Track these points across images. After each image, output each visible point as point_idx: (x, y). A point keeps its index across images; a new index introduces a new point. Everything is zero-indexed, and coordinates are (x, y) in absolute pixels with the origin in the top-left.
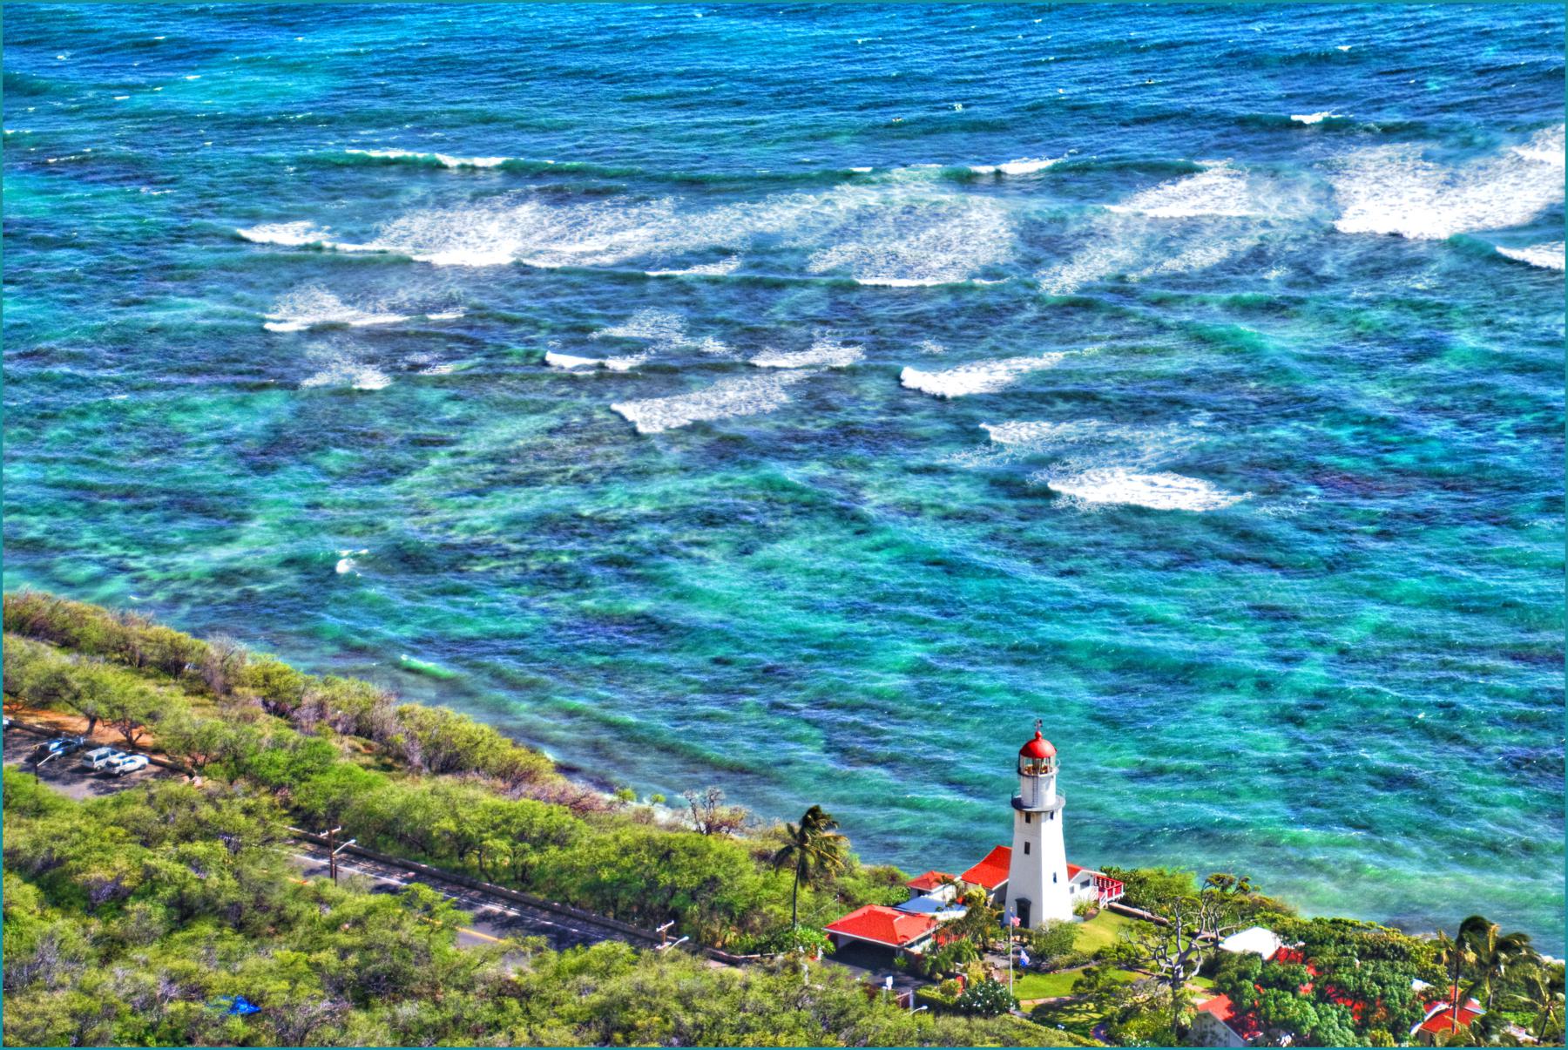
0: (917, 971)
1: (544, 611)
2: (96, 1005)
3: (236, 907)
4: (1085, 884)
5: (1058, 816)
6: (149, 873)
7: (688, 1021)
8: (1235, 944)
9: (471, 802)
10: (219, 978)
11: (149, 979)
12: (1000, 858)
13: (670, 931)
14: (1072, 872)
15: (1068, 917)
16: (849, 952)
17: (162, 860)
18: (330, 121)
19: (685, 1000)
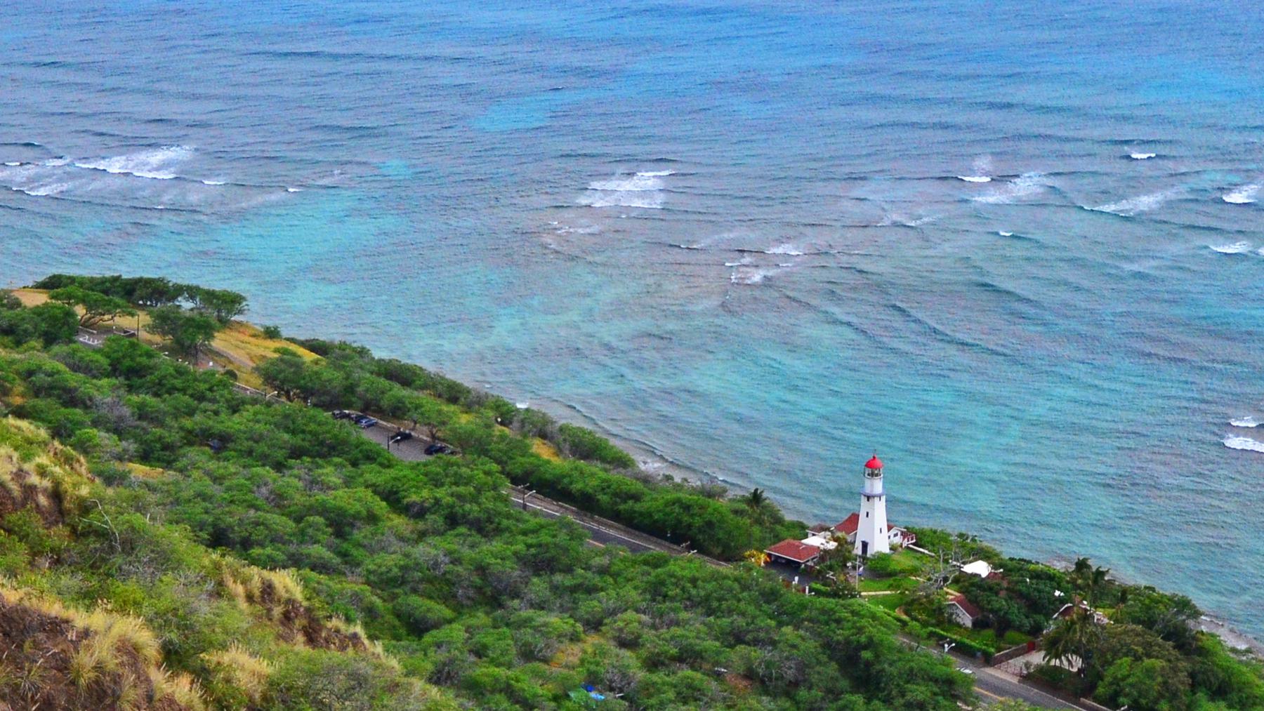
2: (411, 563)
3: (478, 520)
4: (896, 535)
5: (883, 499)
6: (437, 501)
7: (694, 592)
8: (969, 568)
9: (593, 475)
10: (466, 552)
15: (886, 550)
17: (440, 493)
18: (968, 128)
19: (694, 581)
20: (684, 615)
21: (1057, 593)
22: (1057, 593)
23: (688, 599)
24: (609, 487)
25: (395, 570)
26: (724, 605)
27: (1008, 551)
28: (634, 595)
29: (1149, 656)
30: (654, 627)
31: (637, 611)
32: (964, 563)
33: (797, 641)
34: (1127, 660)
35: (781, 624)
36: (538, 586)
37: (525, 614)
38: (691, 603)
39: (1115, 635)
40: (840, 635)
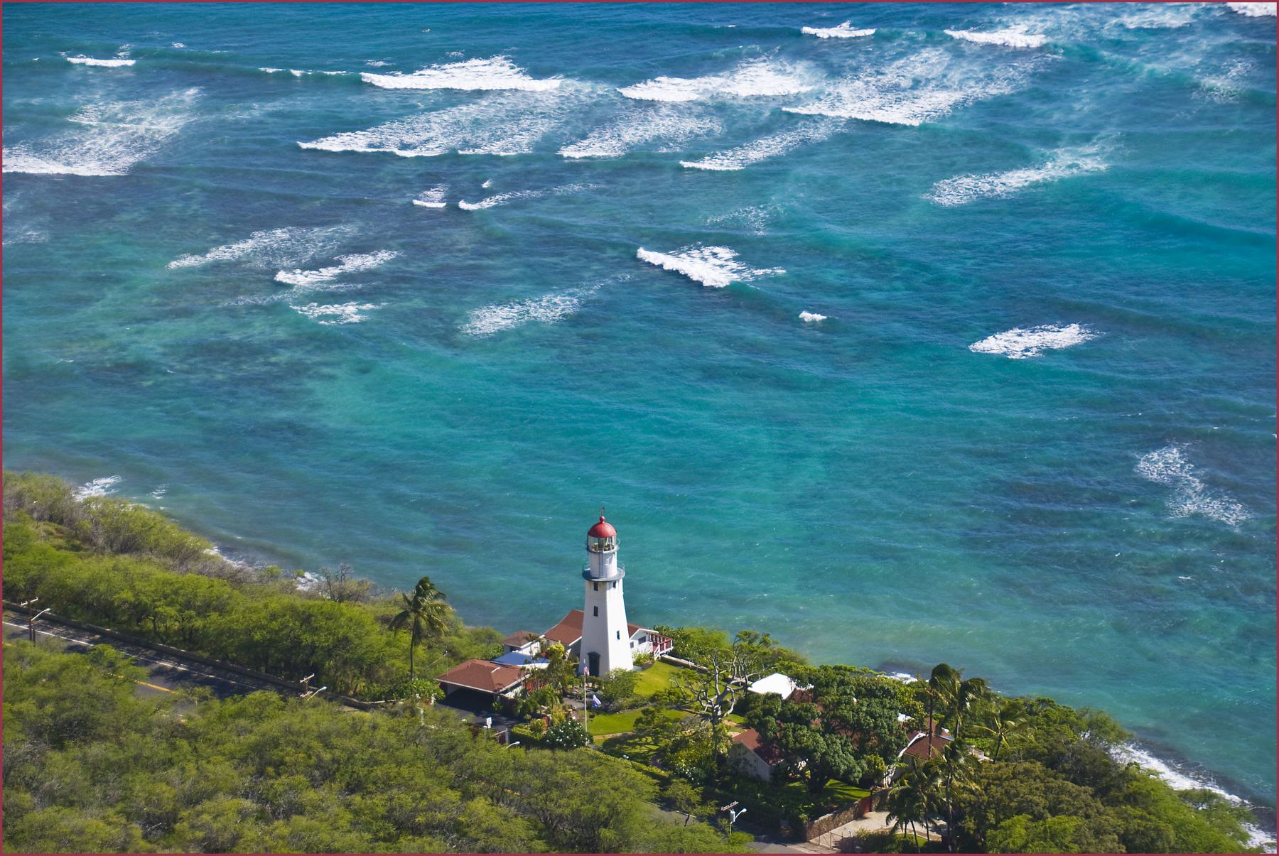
0: (509, 712)
5: (620, 585)
7: (327, 756)
12: (575, 620)
13: (311, 682)
14: (631, 631)
15: (629, 667)
16: (457, 698)
19: (324, 738)
20: (311, 795)
21: (902, 718)
22: (902, 718)
23: (317, 767)
24: (176, 593)
25: (1171, 505)
26: (378, 771)
27: (814, 662)
28: (222, 770)
29: (1054, 811)
30: (261, 817)
31: (234, 793)
32: (754, 679)
33: (496, 821)
34: (1023, 819)
35: (468, 796)
36: (63, 766)
37: (39, 816)
38: (323, 774)
39: (999, 780)
40: (565, 806)
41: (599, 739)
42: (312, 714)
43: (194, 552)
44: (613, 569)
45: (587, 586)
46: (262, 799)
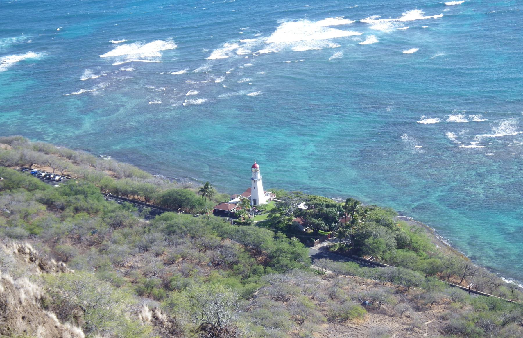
0: (233, 215)
1: (146, 142)
5: (261, 180)
11: (70, 225)
12: (249, 191)
13: (180, 210)
14: (265, 193)
16: (217, 213)
28: (158, 235)
36: (117, 234)
41: (255, 222)
42: (180, 218)
43: (122, 222)
44: (259, 176)
45: (252, 181)
46: (169, 241)
